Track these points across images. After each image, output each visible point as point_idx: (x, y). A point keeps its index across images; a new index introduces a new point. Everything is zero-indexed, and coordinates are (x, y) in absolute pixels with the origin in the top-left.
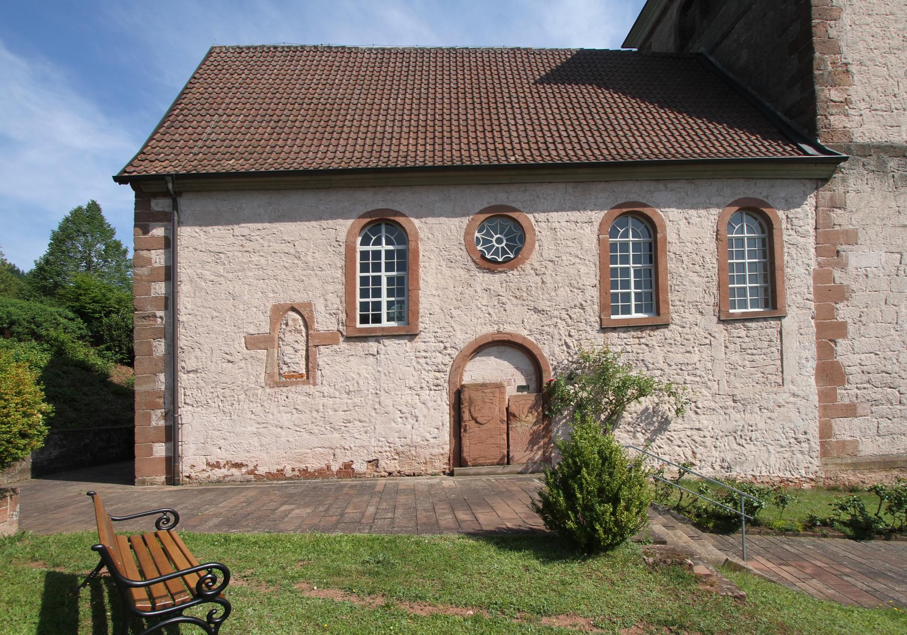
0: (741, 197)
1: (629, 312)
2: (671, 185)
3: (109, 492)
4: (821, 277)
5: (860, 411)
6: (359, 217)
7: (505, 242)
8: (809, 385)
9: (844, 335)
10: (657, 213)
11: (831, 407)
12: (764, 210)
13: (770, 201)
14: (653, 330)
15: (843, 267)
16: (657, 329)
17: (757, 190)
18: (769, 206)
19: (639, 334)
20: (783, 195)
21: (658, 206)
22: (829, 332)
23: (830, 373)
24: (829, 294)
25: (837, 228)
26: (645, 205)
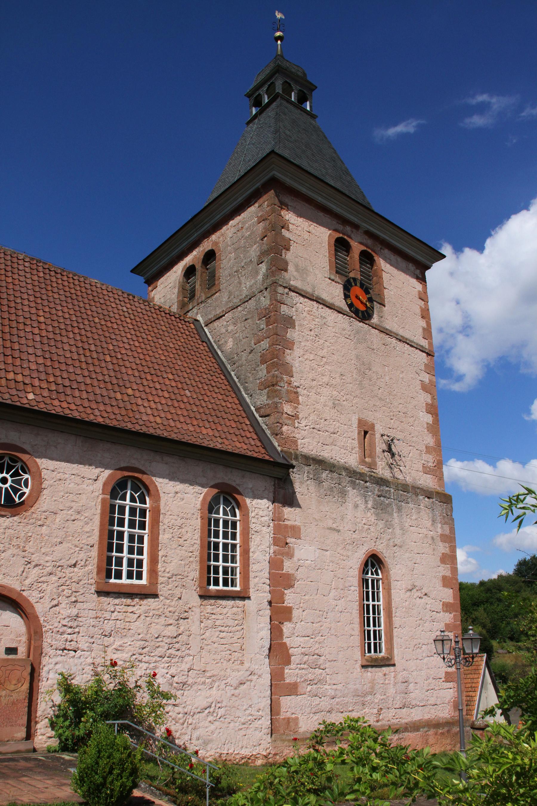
0: (220, 481)
1: (120, 578)
2: (167, 459)
3: (108, 524)
4: (275, 564)
5: (300, 690)
6: (115, 470)
7: (10, 479)
8: (264, 668)
9: (289, 619)
10: (152, 480)
11: (279, 687)
12: (235, 495)
13: (240, 489)
14: (141, 599)
15: (290, 555)
16: (146, 598)
17: (233, 478)
18: (240, 493)
19: (129, 601)
20: (251, 486)
21: (246, 497)
22: (280, 614)
23: (278, 652)
24: (281, 581)
25: (286, 523)
26: (144, 473)
